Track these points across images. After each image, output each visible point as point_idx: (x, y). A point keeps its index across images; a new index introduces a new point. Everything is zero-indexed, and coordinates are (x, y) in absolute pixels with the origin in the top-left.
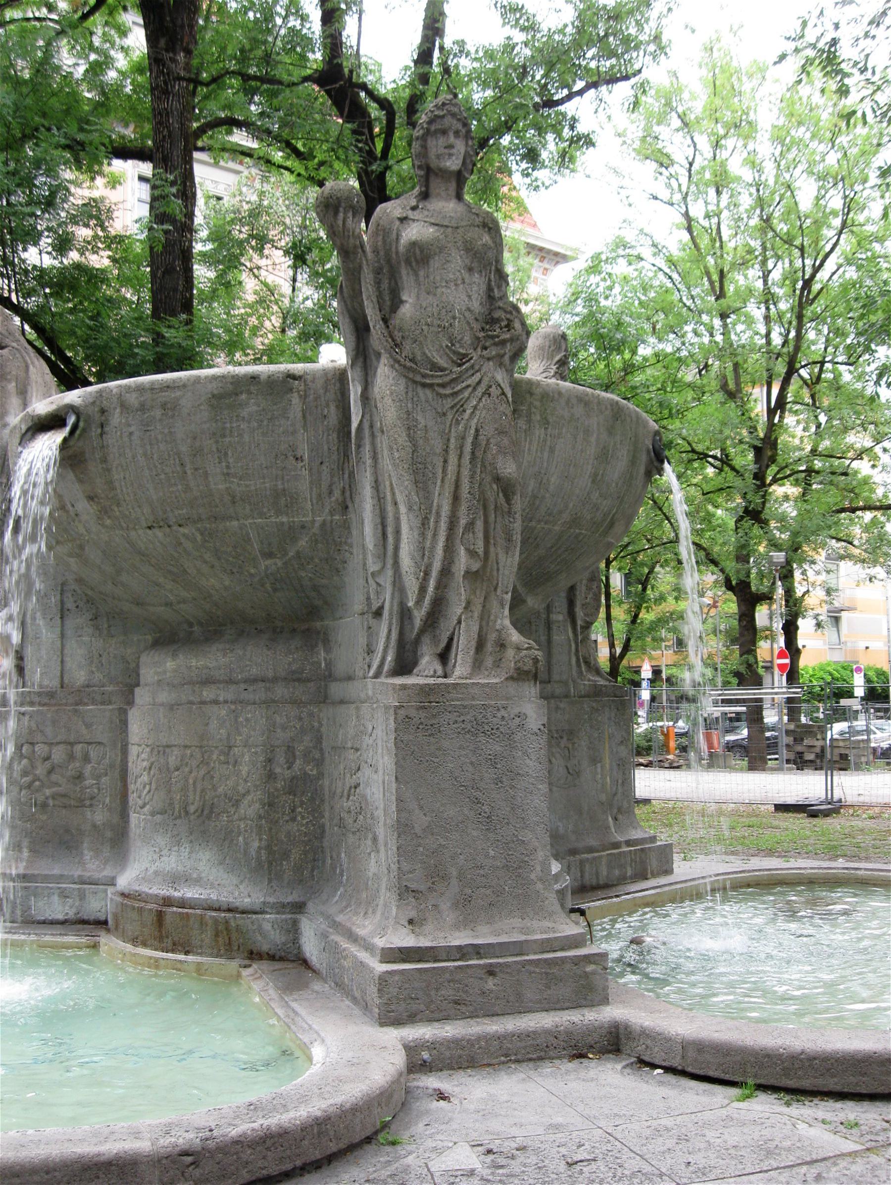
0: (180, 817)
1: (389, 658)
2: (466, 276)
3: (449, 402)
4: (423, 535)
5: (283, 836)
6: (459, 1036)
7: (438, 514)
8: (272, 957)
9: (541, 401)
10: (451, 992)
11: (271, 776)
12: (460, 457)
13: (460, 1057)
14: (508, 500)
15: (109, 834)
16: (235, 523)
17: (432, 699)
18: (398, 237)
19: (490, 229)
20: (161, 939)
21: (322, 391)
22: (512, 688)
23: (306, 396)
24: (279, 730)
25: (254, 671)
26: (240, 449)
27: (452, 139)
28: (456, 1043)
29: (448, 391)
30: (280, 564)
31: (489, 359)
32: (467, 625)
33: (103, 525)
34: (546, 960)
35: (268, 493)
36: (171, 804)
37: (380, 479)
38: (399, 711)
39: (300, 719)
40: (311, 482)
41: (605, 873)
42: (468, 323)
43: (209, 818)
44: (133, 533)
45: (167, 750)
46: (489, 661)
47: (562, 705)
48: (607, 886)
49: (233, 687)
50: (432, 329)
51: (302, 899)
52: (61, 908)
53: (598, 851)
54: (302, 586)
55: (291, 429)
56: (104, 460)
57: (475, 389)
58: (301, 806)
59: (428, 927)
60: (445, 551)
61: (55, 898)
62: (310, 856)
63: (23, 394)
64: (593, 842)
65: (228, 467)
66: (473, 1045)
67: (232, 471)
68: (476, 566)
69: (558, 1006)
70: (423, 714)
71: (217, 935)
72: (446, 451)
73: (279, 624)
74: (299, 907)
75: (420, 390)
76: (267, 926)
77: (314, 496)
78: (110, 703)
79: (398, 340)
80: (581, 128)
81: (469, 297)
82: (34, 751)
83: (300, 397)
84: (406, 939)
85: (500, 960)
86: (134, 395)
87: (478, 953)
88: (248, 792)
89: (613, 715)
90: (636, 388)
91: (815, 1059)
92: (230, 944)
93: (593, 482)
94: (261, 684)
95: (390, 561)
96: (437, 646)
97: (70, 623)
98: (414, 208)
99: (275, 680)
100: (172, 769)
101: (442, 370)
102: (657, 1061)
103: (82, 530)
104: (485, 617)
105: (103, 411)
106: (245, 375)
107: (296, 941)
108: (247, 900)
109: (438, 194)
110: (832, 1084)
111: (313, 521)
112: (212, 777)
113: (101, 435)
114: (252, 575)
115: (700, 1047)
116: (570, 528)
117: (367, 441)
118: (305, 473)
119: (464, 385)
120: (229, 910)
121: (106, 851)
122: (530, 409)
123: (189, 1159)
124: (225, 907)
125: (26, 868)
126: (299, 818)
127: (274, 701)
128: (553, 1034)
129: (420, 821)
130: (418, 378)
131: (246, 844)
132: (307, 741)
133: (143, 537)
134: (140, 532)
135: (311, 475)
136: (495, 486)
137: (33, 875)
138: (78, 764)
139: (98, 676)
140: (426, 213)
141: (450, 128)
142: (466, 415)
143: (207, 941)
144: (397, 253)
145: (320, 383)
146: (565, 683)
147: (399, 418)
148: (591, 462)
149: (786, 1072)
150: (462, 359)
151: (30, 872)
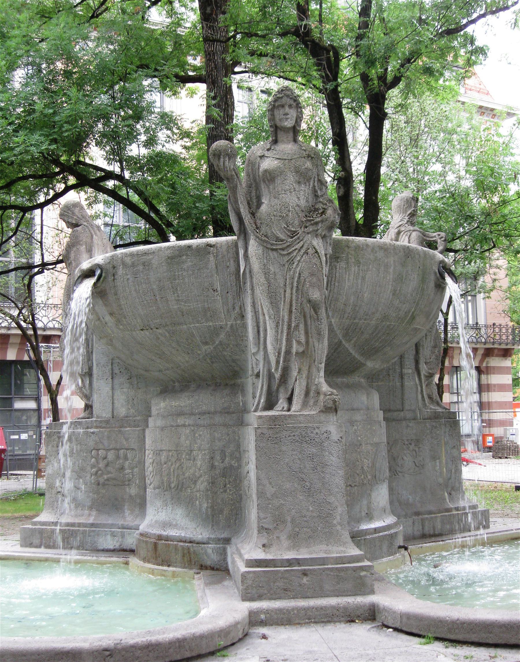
0: (167, 490)
1: (262, 401)
2: (296, 186)
3: (286, 258)
4: (277, 332)
5: (219, 501)
6: (282, 607)
7: (283, 320)
8: (212, 569)
9: (355, 251)
10: (282, 584)
11: (213, 467)
12: (292, 289)
13: (283, 618)
14: (316, 313)
15: (138, 501)
16: (185, 327)
17: (276, 423)
18: (259, 166)
19: (312, 158)
20: (156, 558)
21: (225, 253)
22: (323, 417)
23: (217, 256)
24: (217, 441)
25: (204, 408)
26: (183, 286)
27: (287, 109)
28: (280, 611)
29: (285, 252)
30: (212, 348)
31: (308, 233)
32: (300, 382)
33: (119, 329)
34: (337, 568)
35: (200, 310)
36: (163, 483)
37: (256, 301)
38: (258, 431)
39: (228, 435)
40: (223, 303)
41: (439, 527)
42: (297, 213)
43: (181, 491)
44: (134, 333)
45: (161, 453)
46: (311, 402)
47: (411, 425)
48: (440, 535)
49: (193, 417)
50: (276, 218)
51: (229, 536)
52: (112, 542)
53: (435, 514)
54: (226, 360)
55: (209, 274)
56: (116, 294)
57: (299, 250)
58: (229, 484)
59: (273, 549)
60: (287, 341)
61: (109, 537)
62: (234, 512)
63: (90, 252)
64: (432, 508)
65: (178, 296)
66: (290, 613)
67: (181, 298)
68: (301, 350)
69: (344, 594)
70: (271, 432)
71: (184, 556)
72: (285, 285)
73: (218, 381)
74: (227, 541)
75: (270, 252)
76: (210, 551)
77: (225, 311)
78: (138, 426)
79: (259, 225)
80: (479, 43)
81: (298, 198)
82: (98, 454)
83: (214, 256)
84: (260, 555)
85: (311, 568)
86: (129, 258)
87: (299, 563)
88: (201, 476)
89: (447, 430)
90: (507, 215)
91: (464, 623)
92: (190, 561)
93: (393, 294)
94: (208, 415)
95: (262, 347)
96: (287, 394)
97: (116, 381)
98: (268, 150)
99: (215, 413)
100: (163, 463)
101: (282, 240)
102: (390, 625)
103: (110, 332)
104: (309, 377)
105: (114, 267)
106: (185, 246)
107: (225, 559)
108: (200, 536)
109: (283, 140)
110: (474, 638)
111: (227, 324)
112: (183, 468)
113: (114, 280)
114: (199, 355)
115: (408, 616)
116: (382, 321)
117: (248, 280)
118: (219, 298)
119: (293, 249)
120: (190, 542)
121: (137, 511)
122: (348, 255)
123: (108, 653)
124: (188, 540)
125: (94, 520)
126: (228, 491)
127: (214, 425)
128: (336, 608)
129: (270, 490)
130: (269, 246)
131: (200, 505)
132: (232, 447)
133: (140, 335)
134: (138, 332)
135: (222, 299)
136: (308, 305)
137: (97, 524)
138: (121, 461)
139: (132, 411)
140: (274, 152)
141: (286, 104)
142: (294, 266)
143: (179, 559)
144: (259, 176)
145: (224, 248)
146: (414, 411)
147: (261, 268)
148: (391, 283)
149: (450, 631)
150: (293, 234)
151: (95, 522)
